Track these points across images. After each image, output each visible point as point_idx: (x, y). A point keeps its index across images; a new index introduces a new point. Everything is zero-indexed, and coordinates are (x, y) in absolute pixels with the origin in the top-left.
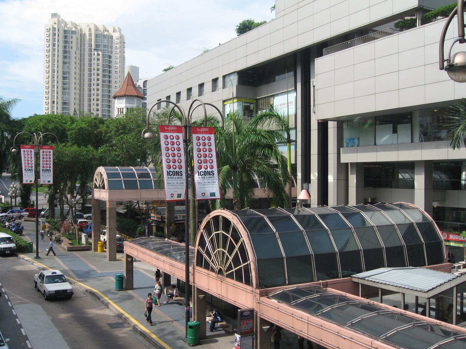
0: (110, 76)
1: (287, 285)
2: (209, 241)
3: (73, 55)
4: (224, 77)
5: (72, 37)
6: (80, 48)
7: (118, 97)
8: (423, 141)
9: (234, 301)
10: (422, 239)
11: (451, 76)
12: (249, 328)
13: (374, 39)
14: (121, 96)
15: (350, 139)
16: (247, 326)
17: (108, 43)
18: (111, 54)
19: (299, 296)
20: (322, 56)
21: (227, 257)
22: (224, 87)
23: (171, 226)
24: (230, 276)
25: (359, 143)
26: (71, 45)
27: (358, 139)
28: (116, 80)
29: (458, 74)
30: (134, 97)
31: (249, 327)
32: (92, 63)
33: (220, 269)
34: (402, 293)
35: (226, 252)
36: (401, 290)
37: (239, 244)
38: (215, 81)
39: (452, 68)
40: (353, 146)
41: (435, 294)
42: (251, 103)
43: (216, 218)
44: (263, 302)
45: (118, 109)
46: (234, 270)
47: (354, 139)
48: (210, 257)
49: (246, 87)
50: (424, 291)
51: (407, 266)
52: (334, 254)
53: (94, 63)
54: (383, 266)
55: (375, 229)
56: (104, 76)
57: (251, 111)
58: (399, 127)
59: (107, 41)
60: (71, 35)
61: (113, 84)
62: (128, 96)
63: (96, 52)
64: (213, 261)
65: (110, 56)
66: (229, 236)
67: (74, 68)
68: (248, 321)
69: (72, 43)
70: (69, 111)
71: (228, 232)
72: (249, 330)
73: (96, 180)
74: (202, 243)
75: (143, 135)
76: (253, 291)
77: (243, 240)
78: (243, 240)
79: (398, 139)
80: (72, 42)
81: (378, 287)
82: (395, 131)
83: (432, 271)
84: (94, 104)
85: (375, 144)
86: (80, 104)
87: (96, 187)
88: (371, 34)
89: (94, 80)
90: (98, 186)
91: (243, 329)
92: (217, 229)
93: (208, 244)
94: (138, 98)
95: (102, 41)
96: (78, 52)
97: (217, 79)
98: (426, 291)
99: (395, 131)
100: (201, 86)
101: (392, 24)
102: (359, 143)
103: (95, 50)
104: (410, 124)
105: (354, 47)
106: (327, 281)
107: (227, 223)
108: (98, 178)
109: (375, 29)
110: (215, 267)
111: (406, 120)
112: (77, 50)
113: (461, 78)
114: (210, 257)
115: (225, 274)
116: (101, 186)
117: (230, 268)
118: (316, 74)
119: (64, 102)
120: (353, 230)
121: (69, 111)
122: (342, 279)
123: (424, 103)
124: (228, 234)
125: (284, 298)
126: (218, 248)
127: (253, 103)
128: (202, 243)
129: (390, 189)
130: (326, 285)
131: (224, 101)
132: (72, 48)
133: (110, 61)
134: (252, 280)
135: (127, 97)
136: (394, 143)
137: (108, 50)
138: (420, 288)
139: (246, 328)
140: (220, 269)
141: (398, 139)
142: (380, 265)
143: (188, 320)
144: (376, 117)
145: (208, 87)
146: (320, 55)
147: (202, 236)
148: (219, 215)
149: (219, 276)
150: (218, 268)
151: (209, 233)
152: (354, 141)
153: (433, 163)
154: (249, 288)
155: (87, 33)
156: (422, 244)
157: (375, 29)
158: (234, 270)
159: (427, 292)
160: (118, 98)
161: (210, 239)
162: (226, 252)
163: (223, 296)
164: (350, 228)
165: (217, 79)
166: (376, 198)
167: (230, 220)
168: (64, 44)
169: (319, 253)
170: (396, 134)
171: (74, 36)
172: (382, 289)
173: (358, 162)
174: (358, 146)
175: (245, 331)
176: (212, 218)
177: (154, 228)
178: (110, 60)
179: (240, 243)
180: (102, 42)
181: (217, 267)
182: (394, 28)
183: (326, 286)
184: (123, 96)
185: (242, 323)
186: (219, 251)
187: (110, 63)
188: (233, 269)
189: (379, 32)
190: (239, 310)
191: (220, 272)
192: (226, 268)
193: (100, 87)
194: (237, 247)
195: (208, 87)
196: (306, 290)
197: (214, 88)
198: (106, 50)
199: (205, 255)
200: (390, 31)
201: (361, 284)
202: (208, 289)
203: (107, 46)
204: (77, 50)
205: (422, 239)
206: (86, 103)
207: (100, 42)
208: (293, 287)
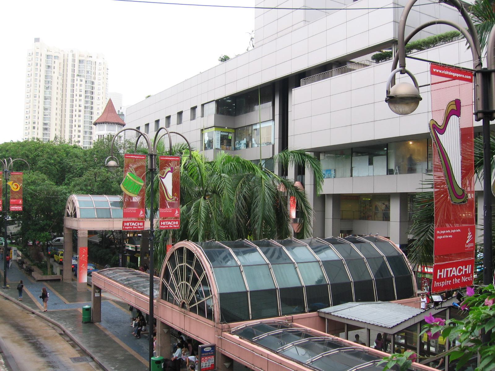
0: (92, 102)
1: (251, 320)
2: (173, 273)
3: (55, 80)
4: (203, 105)
5: (55, 62)
6: (62, 73)
7: (99, 123)
8: (398, 173)
9: (197, 336)
10: (392, 273)
11: (392, 107)
12: (210, 364)
13: (351, 70)
14: (101, 123)
15: (327, 171)
16: (207, 362)
17: (91, 69)
18: (94, 81)
19: (260, 332)
20: (299, 86)
21: (191, 290)
22: (203, 116)
23: (145, 256)
24: (193, 310)
25: (335, 174)
26: (53, 70)
27: (335, 170)
28: (98, 106)
29: (398, 106)
30: (115, 125)
31: (210, 363)
32: (75, 89)
33: (184, 303)
34: (367, 329)
35: (189, 285)
36: (366, 326)
37: (202, 277)
38: (194, 109)
39: (392, 100)
40: (329, 178)
41: (400, 330)
42: (229, 133)
43: (181, 250)
44: (224, 338)
45: (99, 136)
46: (197, 304)
47: (330, 170)
48: (174, 290)
49: (227, 116)
50: (388, 327)
51: (376, 300)
52: (350, 283)
53: (76, 89)
54: (352, 301)
55: (343, 262)
56: (87, 102)
57: (229, 141)
58: (375, 159)
59: (90, 67)
60: (54, 60)
61: (95, 111)
62: (109, 123)
63: (79, 78)
64: (176, 294)
65: (93, 82)
66: (192, 268)
67: (55, 93)
68: (209, 357)
69: (54, 68)
70: (50, 137)
71: (191, 265)
72: (210, 366)
73: (68, 208)
74: (167, 276)
75: (108, 162)
76: (215, 326)
77: (206, 273)
78: (206, 273)
79: (373, 171)
80: (54, 67)
81: (344, 322)
82: (371, 163)
83: (402, 307)
84: (75, 130)
85: (352, 176)
86: (61, 130)
87: (68, 215)
88: (349, 66)
89: (76, 106)
90: (70, 214)
91: (204, 365)
92: (181, 261)
93: (172, 276)
94: (119, 125)
95: (86, 66)
96: (60, 77)
97: (196, 107)
98: (390, 327)
99: (371, 163)
100: (180, 114)
101: (369, 56)
102: (335, 174)
103: (78, 75)
104: (385, 157)
105: (331, 78)
106: (293, 316)
107: (191, 255)
108: (70, 206)
109: (352, 60)
110: (179, 300)
111: (382, 153)
112: (59, 75)
113: (401, 110)
114: (174, 290)
115: (188, 307)
116: (73, 214)
117: (192, 302)
118: (293, 104)
119: (45, 128)
120: (365, 260)
121: (50, 137)
122: (308, 314)
123: (398, 136)
124: (192, 266)
125: (247, 334)
126: (182, 281)
127: (231, 133)
128: (167, 276)
129: (367, 221)
130: (292, 320)
131: (202, 130)
132: (54, 73)
133: (93, 87)
134: (214, 315)
135: (107, 124)
136: (369, 175)
137: (91, 77)
138: (386, 323)
139: (207, 365)
140: (184, 303)
141: (373, 171)
142: (349, 299)
143: (152, 355)
144: (352, 149)
145: (187, 115)
146: (298, 85)
147: (167, 268)
148: (183, 247)
149: (183, 310)
150: (182, 302)
151: (174, 266)
152: (330, 173)
153: (409, 195)
154: (211, 322)
155: (70, 58)
156: (392, 278)
157: (352, 60)
158: (197, 304)
159: (392, 328)
160: (98, 124)
161: (174, 271)
162: (189, 285)
163: (186, 331)
164: (294, 263)
165: (196, 107)
166: (352, 230)
167: (194, 252)
168: (47, 69)
169: (225, 292)
170: (372, 166)
171: (56, 61)
172: (347, 324)
173: (334, 193)
174: (334, 177)
175: (206, 367)
176: (177, 249)
177: (128, 258)
178: (93, 86)
179: (203, 276)
180: (86, 68)
181: (179, 301)
182: (371, 60)
183: (291, 321)
184: (103, 123)
185: (203, 359)
186: (182, 284)
187: (93, 89)
188: (196, 303)
189: (356, 63)
190: (200, 346)
191: (183, 306)
192: (189, 302)
193: (82, 113)
194: (200, 280)
195: (187, 115)
196: (270, 325)
197: (193, 117)
198: (89, 76)
199: (169, 289)
200: (368, 63)
201: (328, 319)
202: (172, 323)
203: (90, 72)
204: (59, 75)
205: (392, 273)
206: (67, 129)
207: (83, 68)
208: (257, 322)
